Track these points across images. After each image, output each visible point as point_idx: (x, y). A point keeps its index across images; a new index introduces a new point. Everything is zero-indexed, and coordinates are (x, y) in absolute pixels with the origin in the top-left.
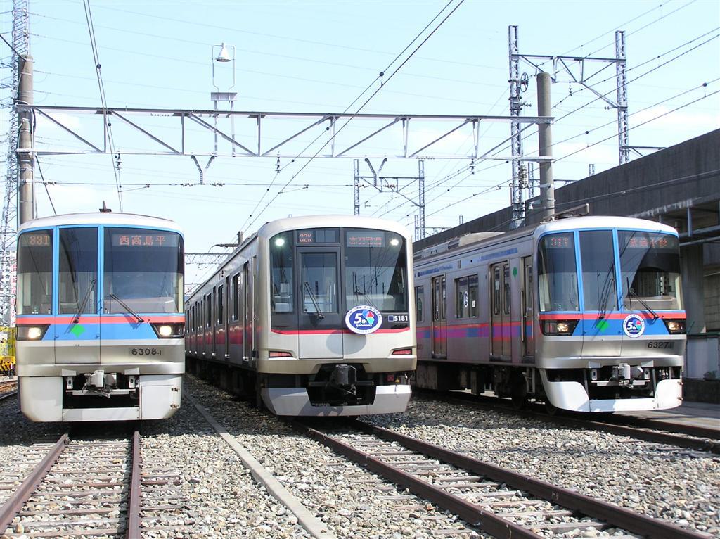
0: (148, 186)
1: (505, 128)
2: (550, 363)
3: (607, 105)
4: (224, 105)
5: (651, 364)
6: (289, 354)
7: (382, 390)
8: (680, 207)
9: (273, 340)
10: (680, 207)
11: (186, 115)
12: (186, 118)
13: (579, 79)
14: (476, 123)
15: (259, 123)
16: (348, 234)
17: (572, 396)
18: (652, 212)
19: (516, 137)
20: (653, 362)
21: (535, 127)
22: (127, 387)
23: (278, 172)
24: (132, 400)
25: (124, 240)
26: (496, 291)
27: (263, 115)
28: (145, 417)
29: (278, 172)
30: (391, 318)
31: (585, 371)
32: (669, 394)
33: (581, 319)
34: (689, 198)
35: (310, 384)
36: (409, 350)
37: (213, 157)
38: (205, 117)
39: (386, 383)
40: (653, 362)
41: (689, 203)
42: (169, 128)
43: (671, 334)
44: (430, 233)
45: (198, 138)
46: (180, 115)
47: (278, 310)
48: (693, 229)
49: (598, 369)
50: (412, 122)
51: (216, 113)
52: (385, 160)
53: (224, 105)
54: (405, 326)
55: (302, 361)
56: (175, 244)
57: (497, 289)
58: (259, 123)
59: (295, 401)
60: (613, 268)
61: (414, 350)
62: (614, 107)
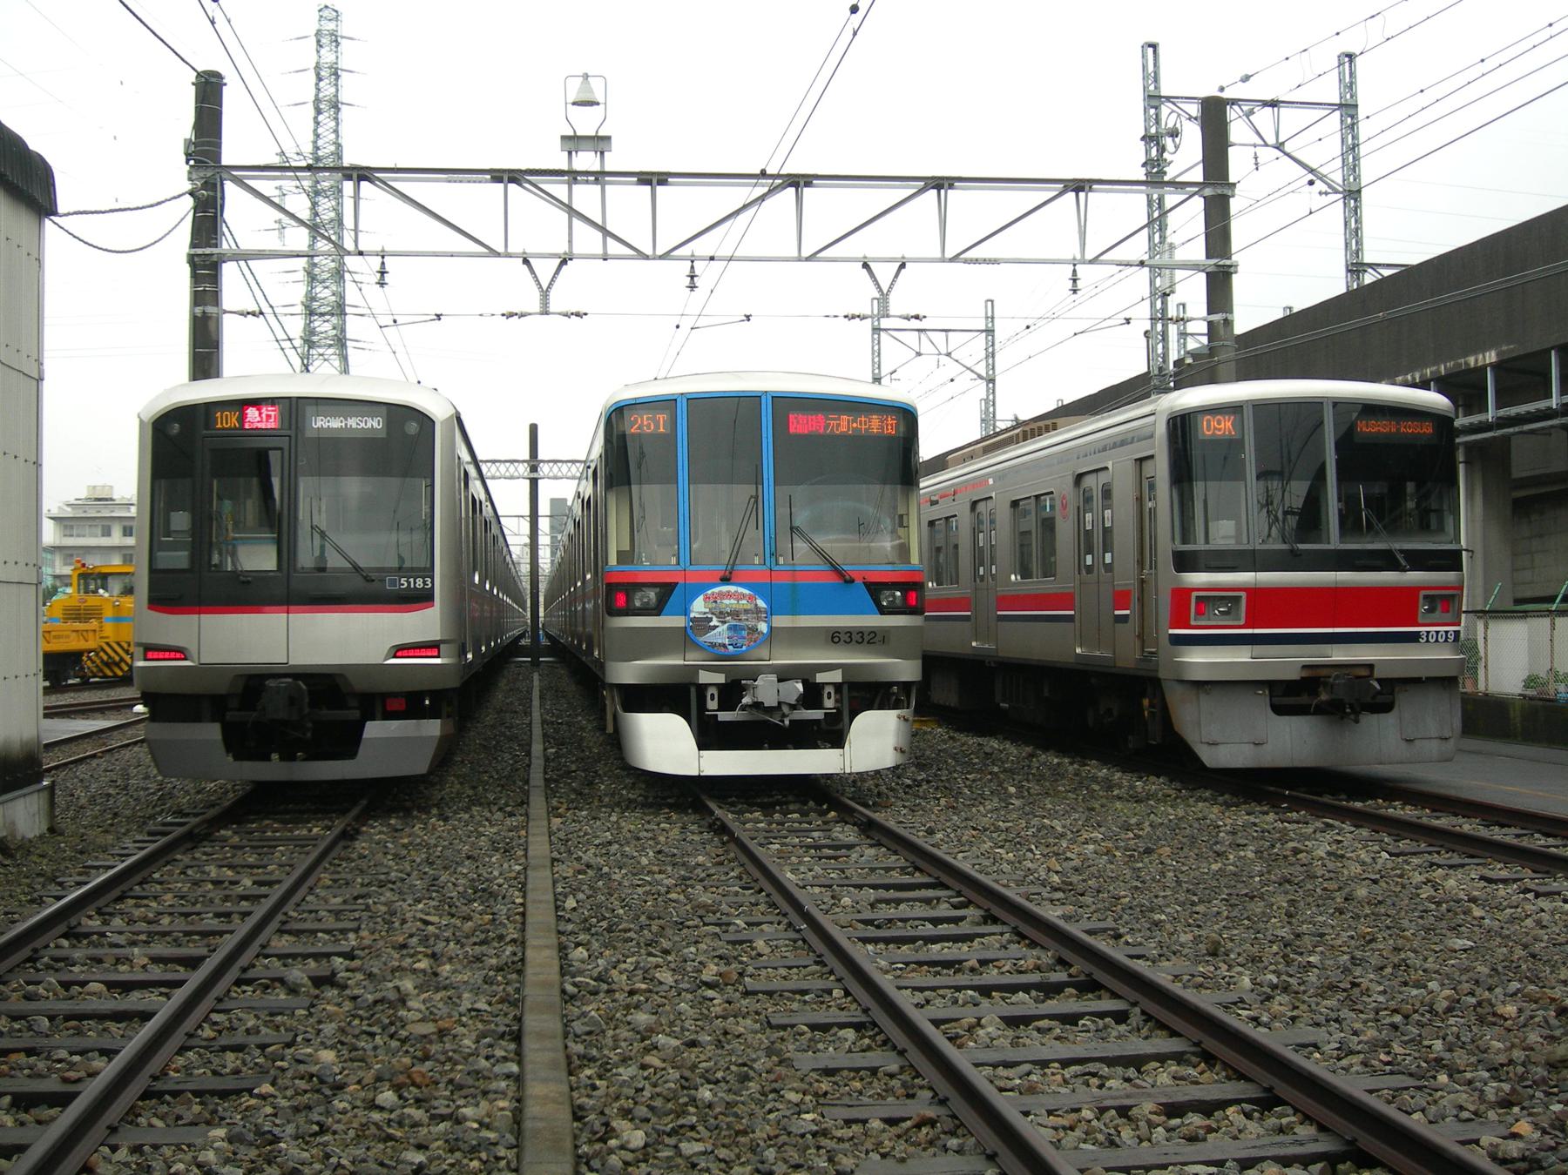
0: (439, 317)
1: (1135, 207)
2: (628, 672)
4: (586, 161)
5: (836, 676)
6: (181, 653)
7: (374, 730)
8: (1472, 364)
10: (1472, 364)
11: (512, 180)
12: (512, 186)
13: (1271, 140)
14: (1082, 195)
15: (799, 199)
16: (310, 410)
17: (665, 743)
18: (1417, 376)
19: (1157, 221)
21: (1198, 204)
23: (1075, 291)
25: (800, 424)
26: (1087, 533)
27: (662, 179)
29: (1075, 291)
30: (393, 583)
31: (693, 690)
32: (875, 740)
33: (681, 582)
34: (1489, 349)
35: (229, 716)
36: (432, 647)
37: (564, 262)
39: (389, 716)
41: (1491, 357)
42: (478, 205)
43: (882, 613)
44: (1004, 419)
45: (535, 221)
46: (649, 183)
47: (161, 566)
48: (1499, 406)
50: (1095, 198)
51: (573, 176)
52: (903, 266)
53: (586, 161)
54: (422, 598)
55: (205, 670)
57: (1089, 527)
58: (799, 199)
60: (758, 480)
62: (1336, 192)
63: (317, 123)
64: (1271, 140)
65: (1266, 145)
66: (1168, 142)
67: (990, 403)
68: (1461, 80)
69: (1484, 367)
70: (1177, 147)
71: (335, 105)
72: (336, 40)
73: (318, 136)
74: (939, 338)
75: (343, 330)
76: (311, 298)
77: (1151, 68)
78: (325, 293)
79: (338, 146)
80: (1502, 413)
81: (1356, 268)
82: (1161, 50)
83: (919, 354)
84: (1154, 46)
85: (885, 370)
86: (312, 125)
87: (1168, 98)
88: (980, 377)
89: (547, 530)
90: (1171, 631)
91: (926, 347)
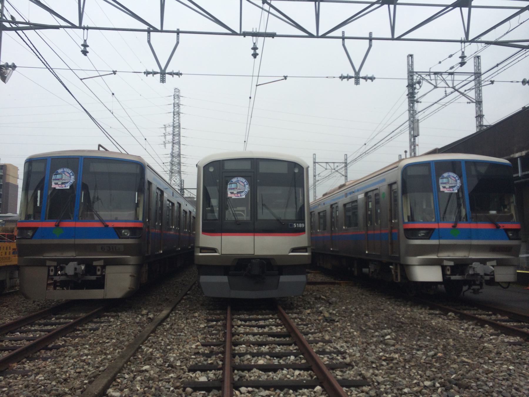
3: (469, 101)
6: (214, 250)
9: (206, 240)
13: (451, 85)
20: (102, 261)
22: (95, 274)
24: (100, 284)
28: (109, 296)
36: (304, 249)
38: (51, 20)
40: (102, 261)
48: (523, 171)
49: (451, 266)
54: (301, 231)
55: (224, 257)
56: (138, 171)
59: (216, 284)
61: (309, 249)
62: (473, 102)
63: (174, 118)
64: (451, 85)
65: (449, 87)
66: (417, 86)
67: (480, 116)
68: (499, 72)
69: (517, 158)
70: (420, 87)
71: (179, 113)
72: (178, 97)
73: (174, 121)
74: (332, 165)
75: (180, 169)
76: (172, 161)
77: (410, 63)
78: (176, 160)
79: (179, 124)
80: (524, 173)
81: (480, 126)
82: (414, 57)
83: (326, 169)
84: (411, 56)
85: (317, 173)
86: (172, 118)
87: (416, 72)
88: (343, 175)
89: (73, 240)
90: (518, 271)
91: (328, 167)
